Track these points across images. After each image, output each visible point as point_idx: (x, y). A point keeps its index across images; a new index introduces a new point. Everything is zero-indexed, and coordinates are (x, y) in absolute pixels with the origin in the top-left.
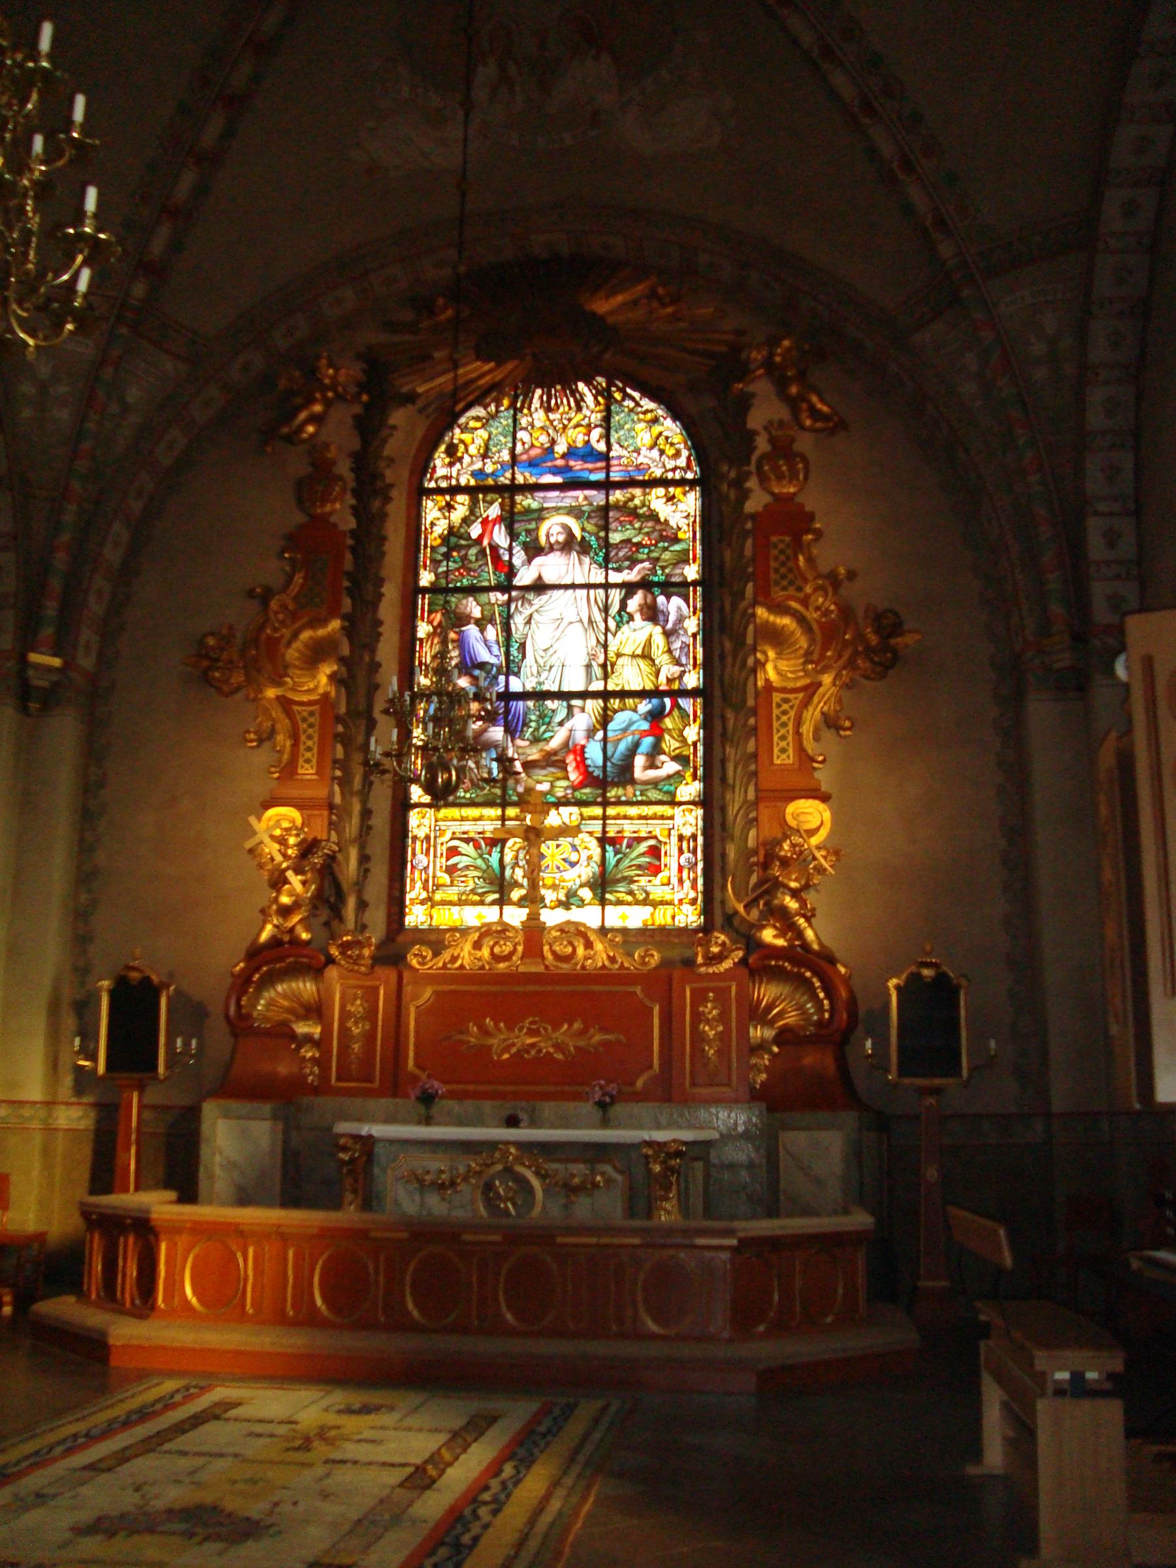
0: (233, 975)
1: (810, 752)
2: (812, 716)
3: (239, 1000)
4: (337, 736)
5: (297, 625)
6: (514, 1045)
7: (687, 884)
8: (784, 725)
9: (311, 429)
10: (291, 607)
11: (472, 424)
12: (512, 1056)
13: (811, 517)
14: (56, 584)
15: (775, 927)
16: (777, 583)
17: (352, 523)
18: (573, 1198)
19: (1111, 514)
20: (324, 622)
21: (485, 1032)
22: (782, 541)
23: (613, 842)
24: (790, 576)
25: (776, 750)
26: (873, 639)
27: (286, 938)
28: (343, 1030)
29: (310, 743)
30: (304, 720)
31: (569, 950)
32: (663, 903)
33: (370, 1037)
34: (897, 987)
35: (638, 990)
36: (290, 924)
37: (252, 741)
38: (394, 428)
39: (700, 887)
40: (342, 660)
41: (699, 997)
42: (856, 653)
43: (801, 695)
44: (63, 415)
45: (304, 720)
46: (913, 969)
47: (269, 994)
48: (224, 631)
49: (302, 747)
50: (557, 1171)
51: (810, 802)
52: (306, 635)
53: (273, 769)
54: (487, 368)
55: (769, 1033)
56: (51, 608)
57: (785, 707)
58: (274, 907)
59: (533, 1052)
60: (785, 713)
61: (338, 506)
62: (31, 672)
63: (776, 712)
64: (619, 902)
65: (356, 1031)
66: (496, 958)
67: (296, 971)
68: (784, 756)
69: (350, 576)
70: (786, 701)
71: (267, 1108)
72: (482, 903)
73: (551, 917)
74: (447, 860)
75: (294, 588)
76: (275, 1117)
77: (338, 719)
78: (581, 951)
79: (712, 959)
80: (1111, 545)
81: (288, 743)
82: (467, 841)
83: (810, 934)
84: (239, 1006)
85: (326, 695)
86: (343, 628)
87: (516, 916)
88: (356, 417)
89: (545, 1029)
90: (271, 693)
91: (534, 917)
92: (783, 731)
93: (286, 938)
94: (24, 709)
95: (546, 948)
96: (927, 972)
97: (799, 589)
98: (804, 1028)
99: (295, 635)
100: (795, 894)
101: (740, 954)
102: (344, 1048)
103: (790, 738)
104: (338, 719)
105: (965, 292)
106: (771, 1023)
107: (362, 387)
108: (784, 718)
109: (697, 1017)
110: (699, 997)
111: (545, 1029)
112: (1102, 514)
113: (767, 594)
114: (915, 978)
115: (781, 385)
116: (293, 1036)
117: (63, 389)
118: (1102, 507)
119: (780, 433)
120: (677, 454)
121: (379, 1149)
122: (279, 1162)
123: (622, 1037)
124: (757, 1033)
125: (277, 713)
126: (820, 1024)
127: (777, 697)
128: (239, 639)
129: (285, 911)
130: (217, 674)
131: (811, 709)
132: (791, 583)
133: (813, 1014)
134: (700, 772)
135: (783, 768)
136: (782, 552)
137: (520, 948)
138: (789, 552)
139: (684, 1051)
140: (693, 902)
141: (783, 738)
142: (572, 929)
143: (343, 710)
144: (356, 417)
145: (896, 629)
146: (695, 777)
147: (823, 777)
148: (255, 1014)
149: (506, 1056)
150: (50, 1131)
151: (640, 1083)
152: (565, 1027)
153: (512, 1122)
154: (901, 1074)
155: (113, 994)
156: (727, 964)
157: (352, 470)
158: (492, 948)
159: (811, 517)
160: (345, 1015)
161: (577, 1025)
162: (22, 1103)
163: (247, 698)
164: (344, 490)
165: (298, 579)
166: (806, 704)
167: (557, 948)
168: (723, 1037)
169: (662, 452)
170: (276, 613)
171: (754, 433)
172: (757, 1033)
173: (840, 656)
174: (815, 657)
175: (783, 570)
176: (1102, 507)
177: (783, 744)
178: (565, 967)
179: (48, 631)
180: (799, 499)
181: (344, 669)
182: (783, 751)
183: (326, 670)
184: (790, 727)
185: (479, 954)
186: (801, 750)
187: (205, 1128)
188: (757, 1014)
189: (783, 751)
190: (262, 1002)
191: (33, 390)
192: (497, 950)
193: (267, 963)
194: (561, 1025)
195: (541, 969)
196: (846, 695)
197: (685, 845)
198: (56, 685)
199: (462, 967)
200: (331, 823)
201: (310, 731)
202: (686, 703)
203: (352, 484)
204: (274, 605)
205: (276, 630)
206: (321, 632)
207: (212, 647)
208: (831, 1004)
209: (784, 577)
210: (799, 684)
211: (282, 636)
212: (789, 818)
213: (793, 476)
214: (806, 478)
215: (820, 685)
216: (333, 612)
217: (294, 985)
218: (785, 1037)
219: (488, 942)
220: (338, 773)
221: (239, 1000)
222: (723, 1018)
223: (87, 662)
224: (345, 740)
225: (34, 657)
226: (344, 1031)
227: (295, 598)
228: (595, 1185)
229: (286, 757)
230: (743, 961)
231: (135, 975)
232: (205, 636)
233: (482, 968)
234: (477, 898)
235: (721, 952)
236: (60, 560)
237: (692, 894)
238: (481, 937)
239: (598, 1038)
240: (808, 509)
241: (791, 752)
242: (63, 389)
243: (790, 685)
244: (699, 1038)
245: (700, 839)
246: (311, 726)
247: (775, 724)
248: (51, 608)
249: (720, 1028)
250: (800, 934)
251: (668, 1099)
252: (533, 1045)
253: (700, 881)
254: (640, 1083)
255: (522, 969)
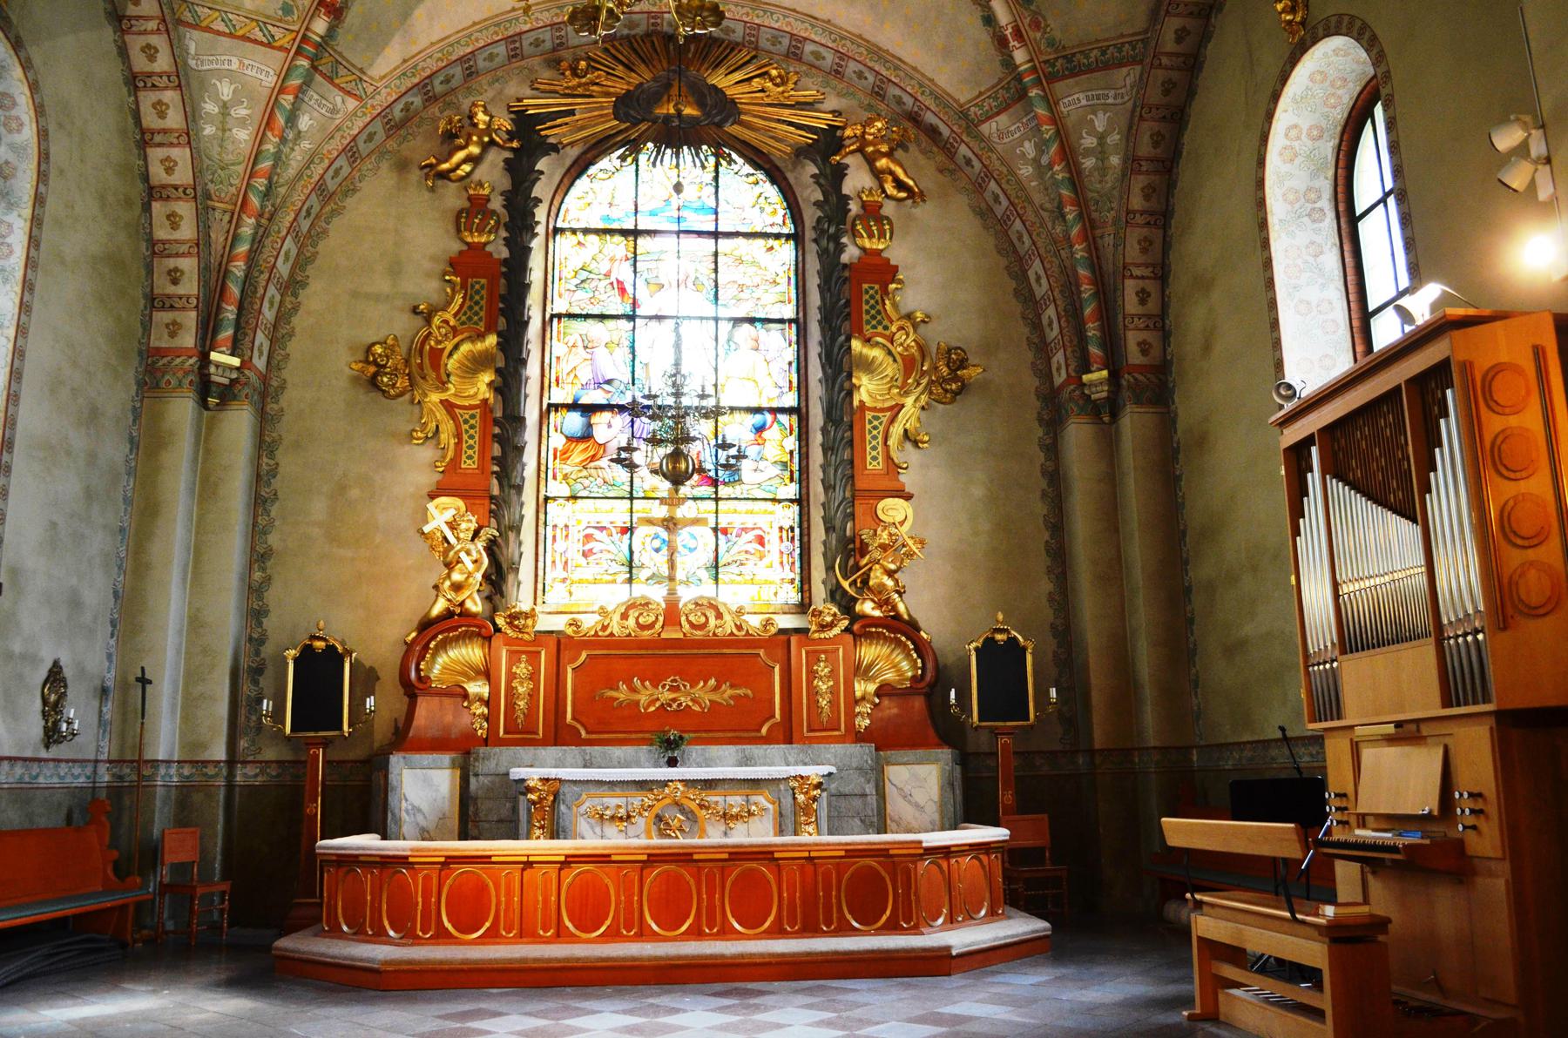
0: (406, 643)
1: (896, 461)
2: (897, 431)
3: (418, 665)
4: (495, 436)
5: (456, 340)
6: (658, 699)
7: (787, 567)
8: (875, 438)
9: (467, 168)
10: (452, 323)
11: (601, 175)
12: (657, 709)
13: (895, 269)
14: (234, 290)
15: (873, 601)
16: (868, 322)
17: (504, 253)
18: (732, 825)
19: (1143, 278)
20: (481, 336)
21: (633, 690)
22: (872, 288)
23: (725, 532)
24: (879, 317)
25: (869, 458)
26: (945, 371)
27: (458, 610)
28: (510, 691)
29: (471, 442)
30: (466, 422)
31: (703, 620)
32: (766, 582)
33: (533, 695)
34: (977, 649)
35: (762, 652)
36: (460, 599)
37: (418, 439)
38: (542, 173)
39: (798, 570)
40: (498, 371)
41: (813, 658)
42: (931, 382)
43: (888, 414)
44: (243, 136)
45: (466, 422)
46: (989, 634)
47: (442, 660)
48: (390, 342)
49: (464, 445)
50: (717, 803)
51: (896, 500)
52: (466, 348)
53: (438, 464)
54: (624, 126)
55: (872, 688)
56: (230, 312)
57: (876, 423)
58: (447, 583)
59: (675, 706)
60: (875, 428)
61: (492, 237)
62: (212, 369)
63: (868, 427)
64: (732, 582)
65: (521, 690)
66: (642, 627)
67: (467, 637)
68: (875, 463)
69: (503, 298)
70: (876, 418)
71: (446, 758)
72: (614, 582)
73: (686, 595)
74: (584, 545)
75: (455, 307)
76: (453, 766)
77: (496, 422)
78: (713, 622)
79: (824, 627)
80: (1143, 302)
81: (453, 441)
82: (602, 529)
83: (901, 608)
84: (418, 670)
85: (485, 401)
86: (498, 343)
87: (657, 594)
88: (506, 161)
89: (685, 686)
90: (435, 397)
91: (672, 592)
92: (874, 443)
93: (458, 610)
94: (203, 404)
95: (683, 619)
96: (999, 637)
97: (886, 328)
98: (901, 683)
99: (456, 347)
100: (890, 574)
101: (846, 622)
102: (511, 706)
103: (880, 449)
104: (496, 422)
105: (1033, 93)
106: (872, 679)
107: (511, 135)
108: (875, 432)
109: (812, 674)
110: (813, 658)
111: (685, 686)
112: (1137, 277)
113: (860, 331)
114: (989, 642)
115: (870, 161)
116: (465, 696)
117: (242, 112)
118: (1137, 272)
119: (870, 199)
120: (775, 212)
121: (565, 789)
122: (457, 809)
123: (749, 692)
124: (860, 688)
125: (441, 414)
126: (914, 678)
127: (869, 415)
128: (403, 350)
129: (457, 587)
130: (385, 379)
131: (896, 425)
132: (880, 323)
133: (906, 671)
134: (796, 475)
135: (875, 475)
136: (872, 297)
137: (661, 619)
138: (878, 297)
139: (801, 703)
140: (792, 581)
141: (874, 448)
142: (705, 602)
143: (499, 414)
144: (506, 161)
145: (963, 363)
146: (792, 480)
147: (907, 479)
148: (432, 676)
149: (652, 709)
150: (230, 787)
151: (764, 731)
152: (702, 684)
153: (672, 763)
154: (980, 720)
155: (296, 660)
156: (836, 631)
157: (504, 206)
158: (637, 619)
159: (895, 269)
160: (511, 676)
161: (712, 682)
162: (205, 763)
163: (412, 401)
164: (498, 223)
165: (459, 299)
166: (892, 421)
167: (692, 618)
168: (834, 691)
169: (762, 210)
170: (439, 328)
171: (848, 198)
172: (860, 688)
173: (919, 384)
174: (899, 383)
175: (873, 312)
176: (1137, 272)
177: (874, 453)
178: (699, 634)
179: (227, 333)
180: (885, 255)
181: (499, 379)
182: (874, 458)
183: (487, 377)
184: (880, 439)
185: (626, 623)
186: (888, 458)
187: (393, 777)
188: (860, 671)
189: (874, 458)
190: (438, 666)
191: (217, 110)
192: (641, 620)
193: (441, 633)
194: (698, 683)
195: (681, 636)
196: (924, 415)
197: (784, 533)
198: (233, 382)
199: (612, 634)
200: (491, 511)
201: (472, 432)
202: (783, 418)
203: (505, 218)
204: (436, 321)
205: (439, 342)
206: (480, 346)
207: (380, 355)
208: (923, 662)
209: (874, 317)
210: (887, 405)
211: (444, 349)
212: (879, 513)
213: (882, 235)
214: (891, 238)
215: (903, 406)
216: (490, 329)
217: (464, 651)
218: (884, 691)
219: (633, 614)
220: (496, 468)
221: (418, 665)
222: (833, 674)
223: (260, 363)
224: (500, 439)
225: (214, 356)
226: (510, 691)
227: (455, 315)
228: (750, 814)
229: (450, 454)
230: (847, 630)
231: (319, 644)
232: (374, 344)
233: (630, 635)
234: (610, 578)
235: (832, 622)
236: (238, 268)
237: (792, 575)
238: (627, 609)
239: (730, 692)
240: (893, 262)
241: (880, 459)
242: (242, 112)
243: (879, 405)
244: (813, 693)
245: (797, 531)
246: (472, 427)
247: (868, 437)
248: (230, 312)
249: (831, 683)
250: (894, 608)
251: (789, 740)
252: (674, 700)
253: (798, 564)
254: (764, 731)
255: (664, 636)
